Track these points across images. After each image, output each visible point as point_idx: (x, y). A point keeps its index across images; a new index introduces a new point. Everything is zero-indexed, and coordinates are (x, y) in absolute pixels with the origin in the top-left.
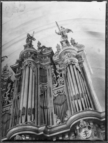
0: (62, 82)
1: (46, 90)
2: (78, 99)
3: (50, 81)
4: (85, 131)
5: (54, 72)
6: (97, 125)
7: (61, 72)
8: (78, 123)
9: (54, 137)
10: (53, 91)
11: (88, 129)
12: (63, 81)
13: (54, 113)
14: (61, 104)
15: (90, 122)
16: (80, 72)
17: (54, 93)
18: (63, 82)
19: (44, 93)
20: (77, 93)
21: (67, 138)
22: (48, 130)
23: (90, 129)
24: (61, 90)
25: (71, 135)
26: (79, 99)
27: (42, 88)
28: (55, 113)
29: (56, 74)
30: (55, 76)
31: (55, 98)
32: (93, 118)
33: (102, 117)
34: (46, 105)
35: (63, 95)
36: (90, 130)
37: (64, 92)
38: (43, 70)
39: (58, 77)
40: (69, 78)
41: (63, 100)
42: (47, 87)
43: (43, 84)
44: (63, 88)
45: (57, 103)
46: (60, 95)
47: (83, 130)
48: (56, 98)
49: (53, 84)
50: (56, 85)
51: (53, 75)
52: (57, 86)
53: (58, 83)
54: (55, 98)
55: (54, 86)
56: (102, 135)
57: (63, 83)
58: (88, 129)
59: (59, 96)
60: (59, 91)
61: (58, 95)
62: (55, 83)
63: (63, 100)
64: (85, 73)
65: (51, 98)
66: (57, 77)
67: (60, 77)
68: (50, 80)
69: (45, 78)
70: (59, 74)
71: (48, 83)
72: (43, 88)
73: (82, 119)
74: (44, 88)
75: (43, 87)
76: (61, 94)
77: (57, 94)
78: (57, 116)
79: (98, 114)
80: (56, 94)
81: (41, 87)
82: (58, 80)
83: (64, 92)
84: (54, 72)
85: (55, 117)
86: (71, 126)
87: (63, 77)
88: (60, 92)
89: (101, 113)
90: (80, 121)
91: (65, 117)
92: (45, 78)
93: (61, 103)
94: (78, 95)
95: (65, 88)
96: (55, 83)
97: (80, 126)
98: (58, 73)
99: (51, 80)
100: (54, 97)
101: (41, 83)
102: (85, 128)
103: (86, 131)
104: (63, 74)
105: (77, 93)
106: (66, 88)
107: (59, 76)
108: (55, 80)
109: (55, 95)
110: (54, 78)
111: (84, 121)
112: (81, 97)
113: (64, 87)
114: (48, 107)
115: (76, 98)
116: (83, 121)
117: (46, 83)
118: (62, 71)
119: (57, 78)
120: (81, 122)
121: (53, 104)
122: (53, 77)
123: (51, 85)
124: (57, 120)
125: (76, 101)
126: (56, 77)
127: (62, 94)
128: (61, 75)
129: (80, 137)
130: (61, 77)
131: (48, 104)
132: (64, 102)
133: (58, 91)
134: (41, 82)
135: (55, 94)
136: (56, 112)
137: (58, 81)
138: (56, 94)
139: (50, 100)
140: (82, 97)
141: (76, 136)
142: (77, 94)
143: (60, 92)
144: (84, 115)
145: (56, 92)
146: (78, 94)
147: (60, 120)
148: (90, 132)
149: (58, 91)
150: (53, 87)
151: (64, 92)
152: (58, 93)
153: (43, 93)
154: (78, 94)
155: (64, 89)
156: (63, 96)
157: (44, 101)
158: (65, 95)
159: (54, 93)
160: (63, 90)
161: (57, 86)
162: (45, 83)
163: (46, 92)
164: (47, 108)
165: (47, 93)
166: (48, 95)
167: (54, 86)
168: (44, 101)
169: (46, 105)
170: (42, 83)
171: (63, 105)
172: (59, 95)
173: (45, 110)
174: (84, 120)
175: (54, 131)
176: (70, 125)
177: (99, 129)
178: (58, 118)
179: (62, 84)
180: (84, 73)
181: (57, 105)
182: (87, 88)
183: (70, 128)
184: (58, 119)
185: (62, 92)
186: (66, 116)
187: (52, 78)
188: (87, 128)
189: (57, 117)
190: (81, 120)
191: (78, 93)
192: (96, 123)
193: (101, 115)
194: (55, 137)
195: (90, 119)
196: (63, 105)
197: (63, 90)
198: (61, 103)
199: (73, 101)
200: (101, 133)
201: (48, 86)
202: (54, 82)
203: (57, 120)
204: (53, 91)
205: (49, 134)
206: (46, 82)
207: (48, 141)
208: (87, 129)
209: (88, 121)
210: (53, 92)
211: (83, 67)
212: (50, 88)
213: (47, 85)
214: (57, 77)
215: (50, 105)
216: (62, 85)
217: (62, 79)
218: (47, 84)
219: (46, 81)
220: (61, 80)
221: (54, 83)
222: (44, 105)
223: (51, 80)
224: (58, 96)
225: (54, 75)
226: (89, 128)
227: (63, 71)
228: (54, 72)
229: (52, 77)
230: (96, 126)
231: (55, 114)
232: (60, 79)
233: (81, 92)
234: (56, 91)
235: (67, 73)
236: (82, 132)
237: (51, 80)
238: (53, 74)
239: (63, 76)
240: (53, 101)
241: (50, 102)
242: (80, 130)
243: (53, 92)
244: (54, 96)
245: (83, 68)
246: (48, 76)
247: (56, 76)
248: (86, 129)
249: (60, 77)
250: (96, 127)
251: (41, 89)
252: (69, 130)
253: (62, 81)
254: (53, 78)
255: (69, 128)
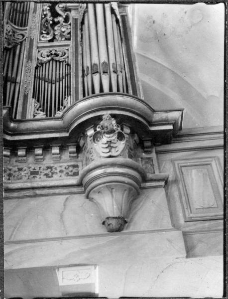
0: (65, 34)
1: (21, 43)
2: (104, 72)
3: (35, 25)
4: (108, 141)
5: (49, 10)
6: (136, 138)
7: (68, 12)
8: (94, 122)
9: (21, 146)
10: (38, 47)
11: (118, 138)
12: (69, 33)
13: (30, 95)
14: (54, 82)
15: (124, 126)
16: (117, 21)
17: (40, 53)
18: (69, 35)
19: (15, 47)
20: (104, 58)
21: (56, 154)
22: (12, 125)
23: (121, 140)
24: (60, 51)
25: (68, 149)
26: (107, 73)
27: (11, 33)
28: (33, 97)
29: (55, 14)
30: (49, 18)
31: (40, 65)
32: (136, 117)
33: (155, 122)
34: (14, 75)
35: (63, 62)
36: (122, 142)
37: (66, 55)
38: (12, 18)
39: (59, 22)
40: (89, 27)
41: (59, 74)
42: (23, 37)
43: (17, 27)
44: (67, 48)
45: (44, 76)
46: (56, 61)
47: (105, 139)
48: (44, 65)
49: (42, 33)
50: (49, 37)
51: (46, 15)
52: (50, 41)
53: (54, 35)
54: (42, 64)
55: (43, 39)
56: (143, 162)
57: (67, 38)
58: (116, 139)
59: (51, 62)
60: (53, 52)
61: (50, 58)
62: (48, 34)
63: (59, 74)
64: (128, 29)
65: (30, 62)
66: (56, 20)
67: (64, 22)
68: (35, 21)
69: (23, 16)
70: (60, 15)
71: (27, 28)
72: (14, 36)
73: (110, 112)
74: (16, 36)
75: (14, 32)
76: (57, 58)
77: (48, 56)
78: (38, 105)
79: (149, 111)
80: (45, 56)
81: (9, 32)
82: (56, 28)
83: (68, 57)
84: (48, 8)
85: (33, 106)
86: (75, 125)
87: (70, 24)
88: (57, 55)
89: (154, 111)
90: (103, 115)
91: (59, 108)
92: (23, 16)
93: (54, 78)
94: (106, 64)
95: (71, 49)
96: (46, 32)
97: (98, 130)
98: (60, 12)
99: (38, 25)
100: (40, 61)
101: (9, 21)
102: (112, 135)
103: (110, 142)
104: (73, 18)
105: (104, 58)
106: (74, 50)
107: (61, 19)
108: (48, 27)
109: (41, 58)
110: (47, 21)
111: (113, 119)
112: (112, 70)
113: (68, 45)
114: (18, 80)
115: (99, 71)
116: (110, 116)
117: (23, 28)
118: (70, 10)
119: (55, 24)
120: (103, 117)
121: (33, 76)
122: (43, 18)
123: (35, 34)
124: (36, 113)
125: (96, 78)
126: (53, 20)
127: (62, 59)
128: (66, 20)
129: (90, 154)
130: (64, 24)
131: (19, 74)
132: (63, 78)
133: (51, 51)
134: (12, 21)
135: (41, 56)
136: (36, 95)
137: (54, 30)
138: (45, 56)
139: (26, 66)
140: (115, 72)
141: (79, 155)
142: (102, 61)
143: (57, 55)
144: (118, 103)
145: (47, 52)
146: (106, 63)
147: (45, 113)
148: (121, 145)
149: (51, 51)
150: (40, 40)
151: (68, 57)
152: (52, 54)
153: (10, 47)
154: (104, 63)
155: (68, 50)
156: (61, 64)
157: (11, 64)
158: (69, 63)
159: (40, 53)
160: (66, 51)
161: (50, 41)
162: (21, 26)
163: (19, 46)
164: (15, 83)
165: (21, 48)
166: (25, 54)
167: (43, 39)
168: (11, 64)
169: (14, 75)
170: (13, 25)
171: (58, 84)
172: (52, 59)
173: (9, 84)
174: (113, 116)
175: (27, 129)
176: (72, 124)
177: (140, 150)
178: (41, 109)
179: (64, 39)
180: (126, 29)
181: (43, 82)
182: (127, 59)
183: (70, 131)
184: (39, 112)
185: (60, 56)
186: (61, 107)
187: (42, 20)
188: (116, 135)
189: (38, 106)
190: (106, 114)
191: (106, 61)
192: (137, 133)
193: (153, 117)
194: (23, 146)
195: (128, 116)
196: (58, 84)
197: (66, 51)
198: (54, 78)
199: (89, 76)
200: (142, 158)
201: (26, 35)
202: (45, 31)
203: (36, 113)
204: (38, 47)
205: (12, 135)
206: (25, 26)
207: (77, 33)
208: (114, 137)
209: (121, 120)
210: (39, 52)
211: (126, 15)
212: (31, 41)
213: (27, 31)
214: (56, 20)
215: (24, 76)
216: (65, 40)
217: (67, 29)
218: (26, 29)
219: (23, 23)
220: (63, 30)
221: (44, 32)
222: (9, 75)
223: (38, 25)
224: (49, 61)
225: (49, 14)
226: (121, 137)
227: (73, 12)
228: (48, 8)
229: (42, 18)
230: (135, 139)
231: (34, 100)
232: (62, 26)
233: (112, 61)
234: (47, 50)
235: (86, 14)
236: (100, 142)
237: (38, 25)
238: (45, 13)
239: (71, 21)
240: (34, 70)
241: (26, 71)
242: (95, 138)
243: (39, 52)
244: (38, 59)
245: (126, 17)
246: (31, 13)
247: (51, 18)
248: (113, 136)
249: (64, 22)
250: (135, 140)
251: (9, 37)
252: (66, 135)
253: (69, 31)
254: (44, 21)
255: (68, 131)
